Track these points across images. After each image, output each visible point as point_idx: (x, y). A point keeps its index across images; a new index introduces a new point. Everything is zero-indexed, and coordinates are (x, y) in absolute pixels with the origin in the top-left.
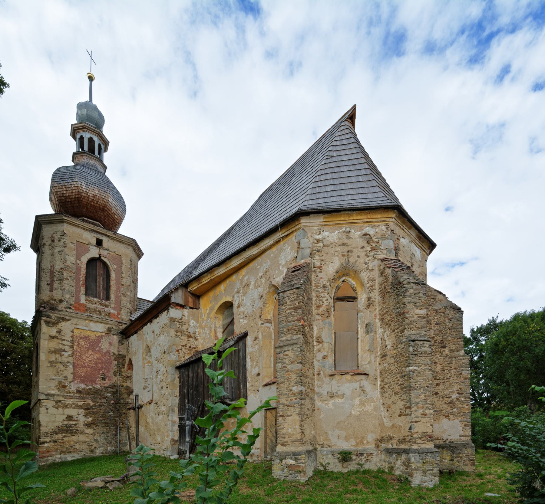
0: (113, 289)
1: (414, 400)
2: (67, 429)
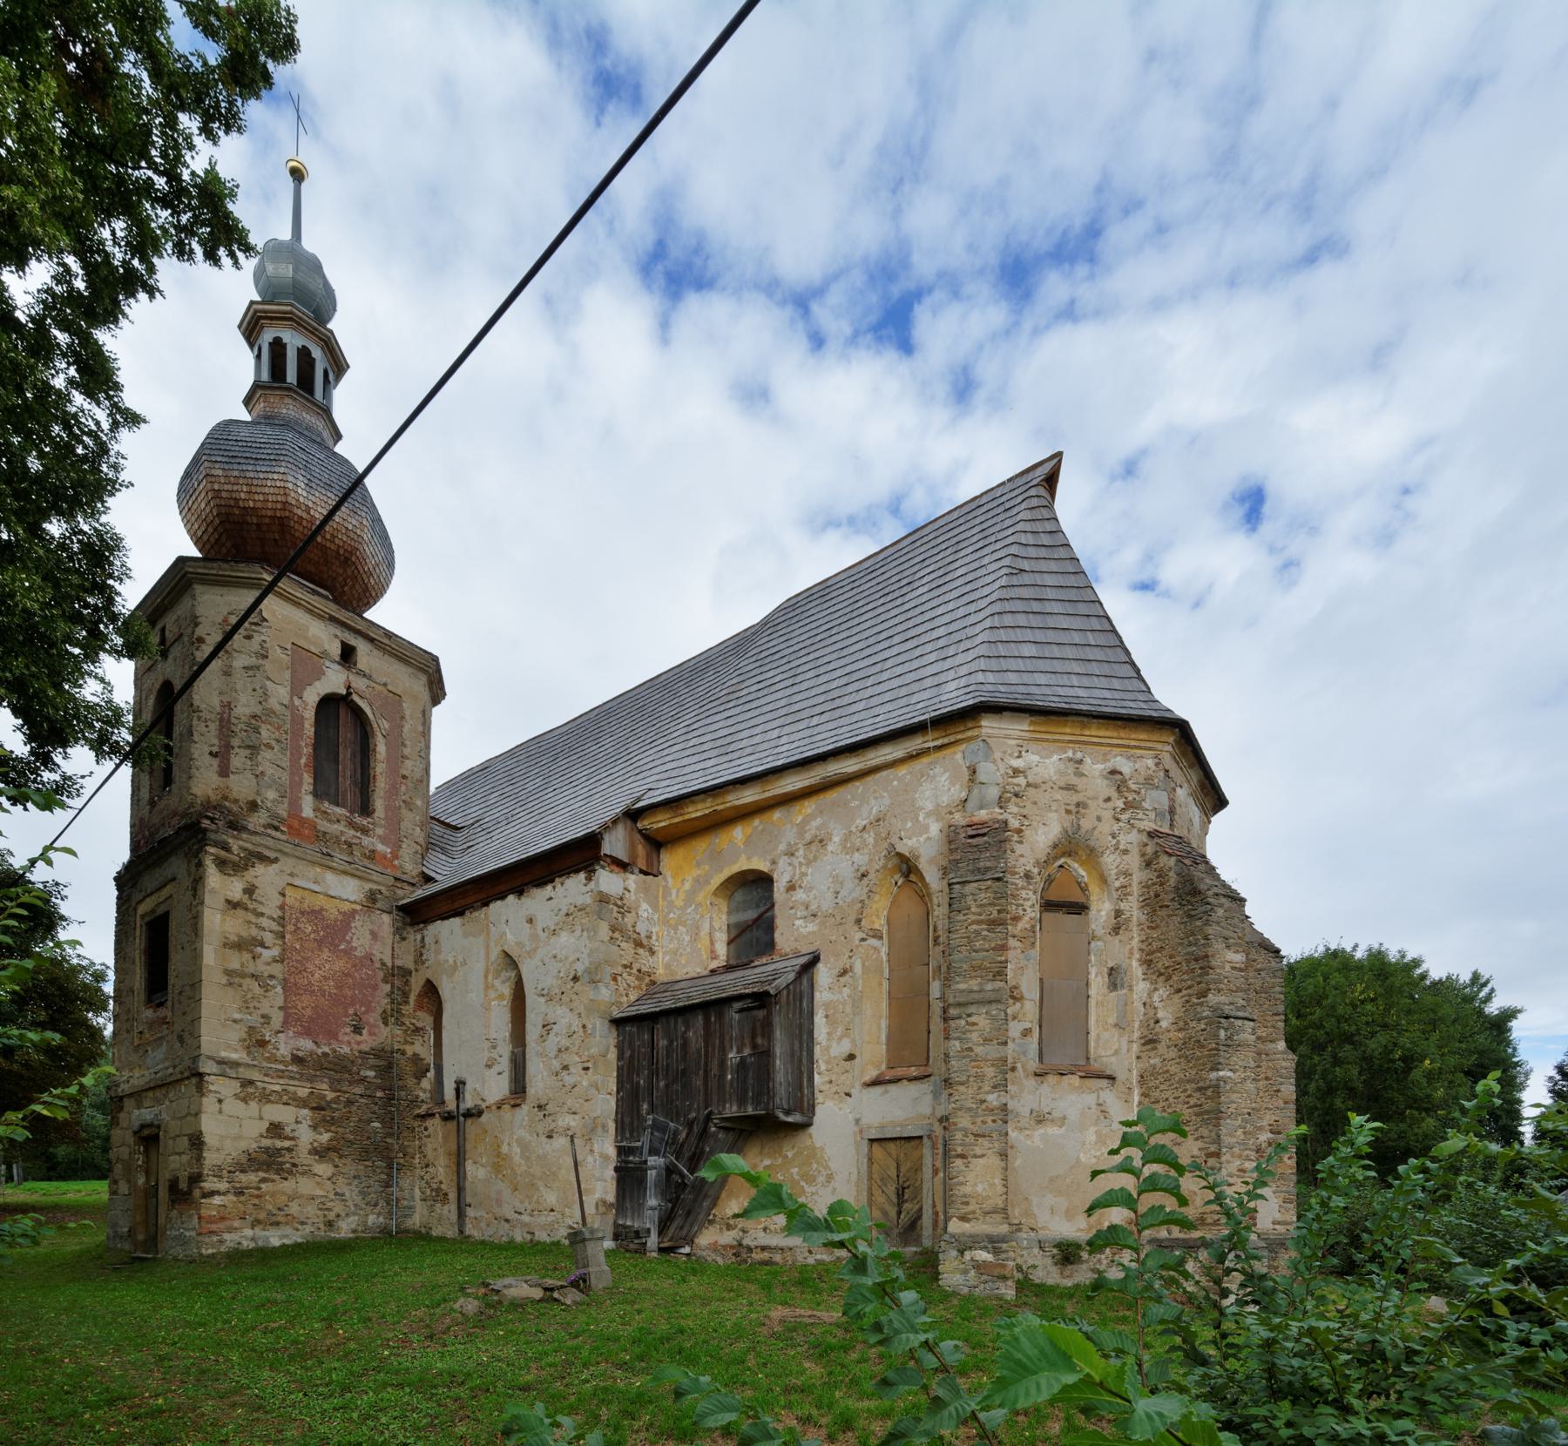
0: (381, 785)
1: (1226, 1140)
2: (270, 1160)
